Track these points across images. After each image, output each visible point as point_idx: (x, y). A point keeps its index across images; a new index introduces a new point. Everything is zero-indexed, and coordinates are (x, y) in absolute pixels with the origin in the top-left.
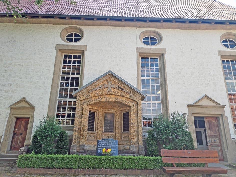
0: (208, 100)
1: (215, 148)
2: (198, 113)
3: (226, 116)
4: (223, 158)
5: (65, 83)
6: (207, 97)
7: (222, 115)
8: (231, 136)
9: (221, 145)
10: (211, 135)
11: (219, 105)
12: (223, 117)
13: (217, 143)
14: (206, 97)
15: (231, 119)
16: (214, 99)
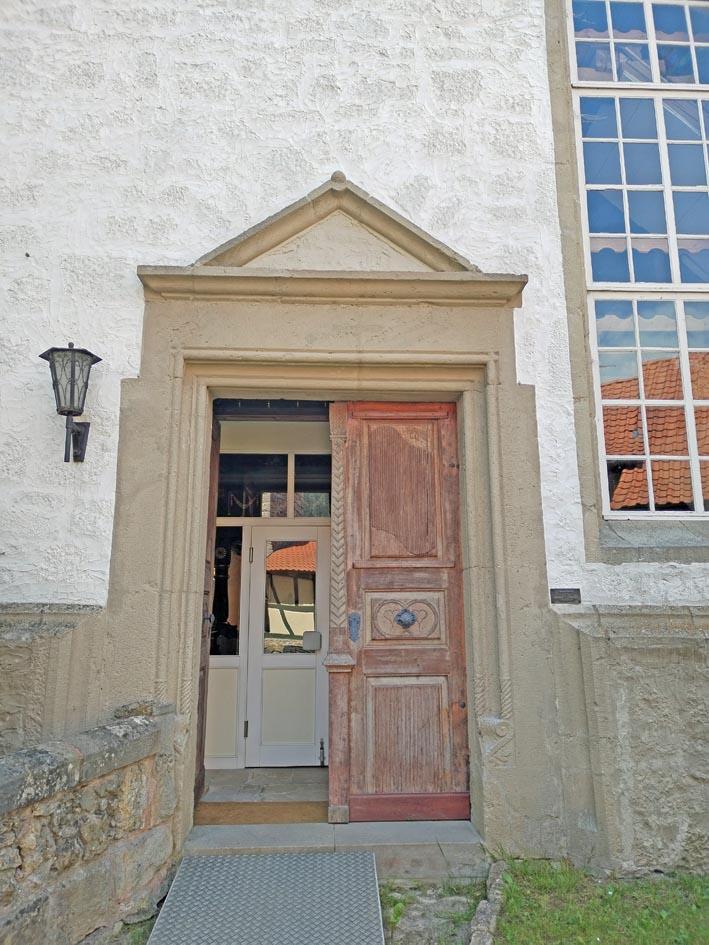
0: (363, 233)
1: (397, 688)
2: (289, 356)
3: (521, 378)
4: (460, 789)
5: (658, 457)
6: (346, 203)
7: (482, 367)
8: (544, 575)
9: (460, 665)
10: (379, 564)
11: (459, 276)
12: (491, 389)
13: (428, 645)
14: (341, 197)
15: (571, 408)
16: (422, 220)
